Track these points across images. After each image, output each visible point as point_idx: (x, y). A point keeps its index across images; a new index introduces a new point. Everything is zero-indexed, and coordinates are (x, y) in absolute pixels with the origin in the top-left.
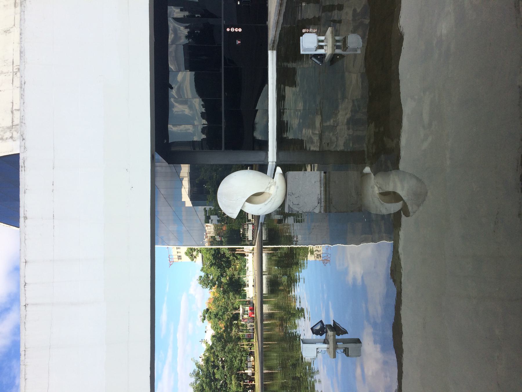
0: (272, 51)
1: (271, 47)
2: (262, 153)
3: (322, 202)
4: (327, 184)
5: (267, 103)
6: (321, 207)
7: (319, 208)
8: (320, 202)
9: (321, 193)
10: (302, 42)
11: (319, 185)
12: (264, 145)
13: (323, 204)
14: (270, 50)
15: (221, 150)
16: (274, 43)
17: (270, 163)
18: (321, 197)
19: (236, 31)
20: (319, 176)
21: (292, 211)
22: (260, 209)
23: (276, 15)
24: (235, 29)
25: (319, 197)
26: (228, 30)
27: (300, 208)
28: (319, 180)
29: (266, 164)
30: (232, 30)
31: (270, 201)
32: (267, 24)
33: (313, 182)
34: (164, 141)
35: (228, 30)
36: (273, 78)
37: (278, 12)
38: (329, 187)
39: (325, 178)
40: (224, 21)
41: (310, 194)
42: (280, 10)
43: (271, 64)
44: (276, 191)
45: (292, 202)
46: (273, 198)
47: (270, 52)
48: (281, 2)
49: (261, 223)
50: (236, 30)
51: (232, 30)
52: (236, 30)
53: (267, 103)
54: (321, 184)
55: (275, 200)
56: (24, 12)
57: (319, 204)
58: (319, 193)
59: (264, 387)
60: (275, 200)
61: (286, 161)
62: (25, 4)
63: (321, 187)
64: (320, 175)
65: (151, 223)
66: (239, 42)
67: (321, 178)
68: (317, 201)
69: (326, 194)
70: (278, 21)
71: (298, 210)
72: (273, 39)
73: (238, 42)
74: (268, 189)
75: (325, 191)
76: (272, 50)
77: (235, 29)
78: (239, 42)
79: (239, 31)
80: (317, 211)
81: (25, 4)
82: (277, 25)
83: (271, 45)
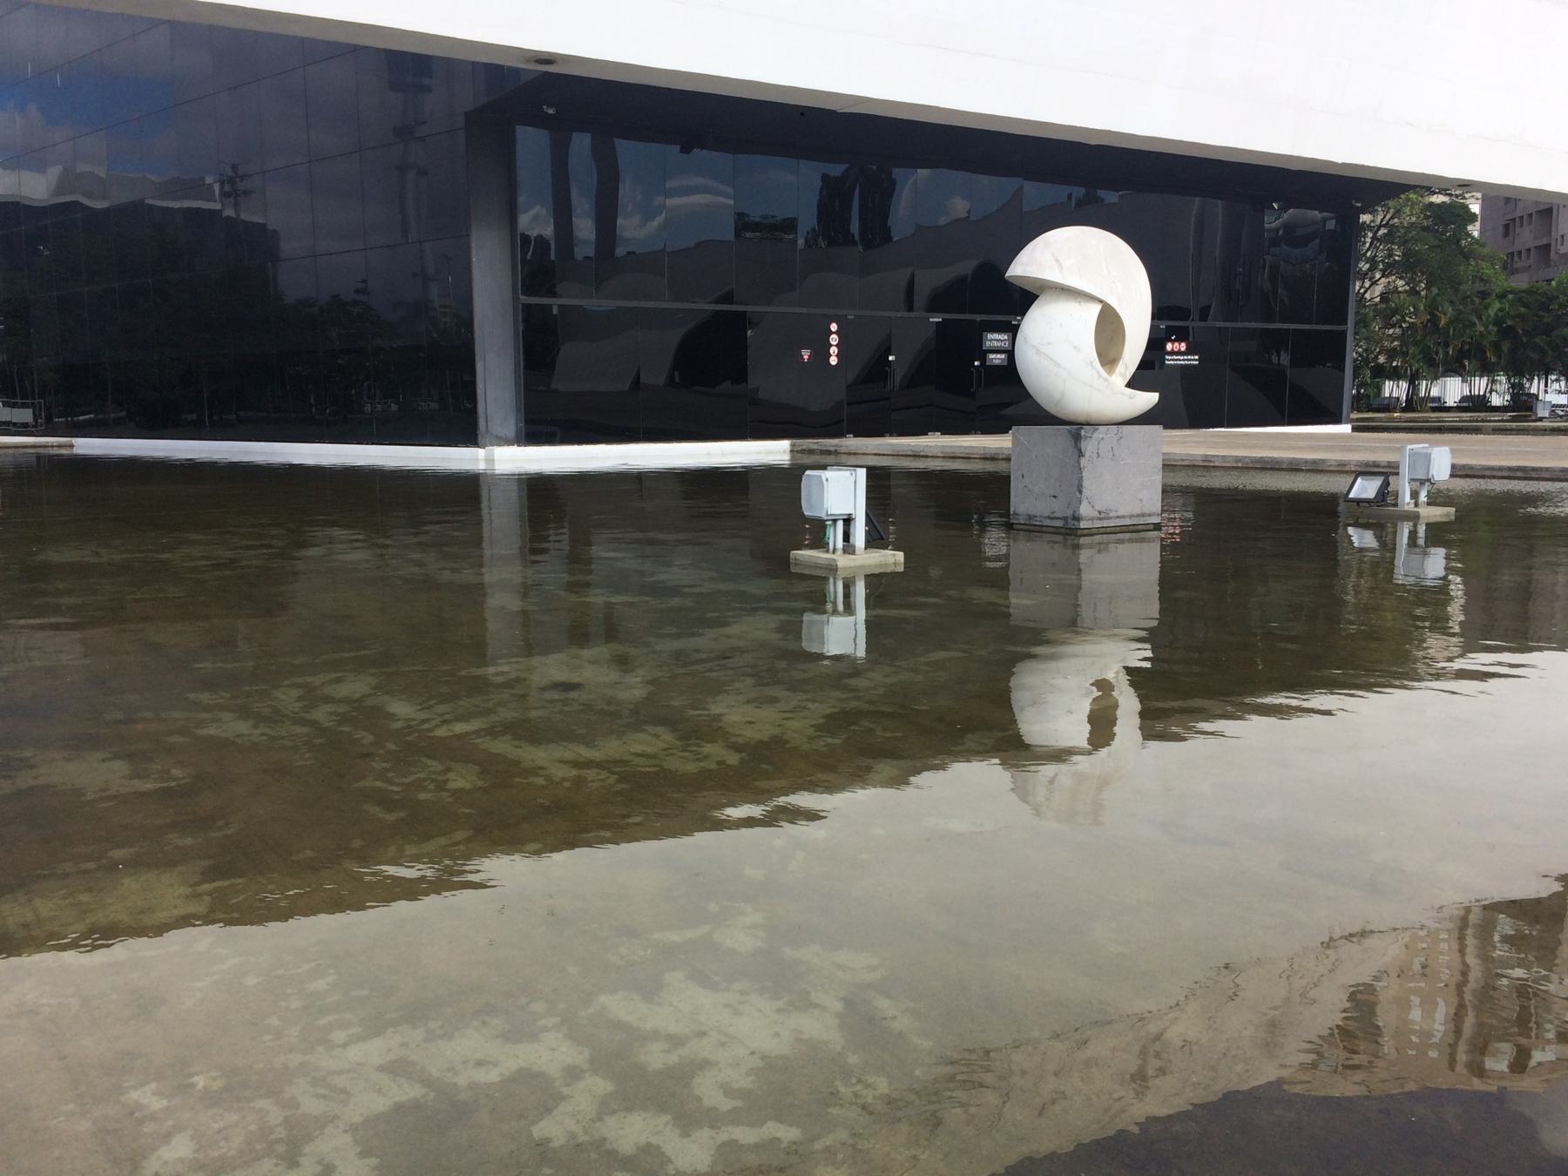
0: (789, 449)
1: (804, 447)
2: (510, 429)
3: (1101, 522)
4: (1135, 531)
5: (376, 442)
6: (1092, 519)
7: (1091, 515)
8: (1103, 515)
9: (1118, 517)
11: (1134, 513)
12: (535, 432)
13: (1098, 524)
15: (527, 291)
18: (1111, 518)
19: (831, 351)
21: (1086, 437)
22: (1075, 348)
23: (948, 450)
24: (832, 345)
25: (1111, 515)
26: (834, 327)
27: (1090, 465)
28: (1146, 511)
29: (480, 439)
30: (834, 339)
31: (1100, 375)
32: (848, 436)
35: (834, 327)
36: (723, 455)
37: (961, 453)
38: (1131, 541)
40: (852, 317)
41: (1118, 488)
42: (969, 458)
45: (1103, 439)
46: (1106, 383)
48: (1002, 459)
49: (72, 446)
50: (834, 350)
51: (834, 339)
52: (834, 350)
53: (376, 442)
54: (1138, 516)
55: (1100, 390)
57: (1098, 515)
58: (1119, 514)
59: (1567, 421)
60: (1100, 390)
61: (489, 496)
63: (1131, 517)
66: (806, 357)
67: (1150, 515)
68: (1104, 510)
70: (923, 456)
72: (844, 448)
73: (806, 354)
76: (792, 451)
77: (832, 345)
78: (806, 357)
82: (906, 456)
83: (816, 447)
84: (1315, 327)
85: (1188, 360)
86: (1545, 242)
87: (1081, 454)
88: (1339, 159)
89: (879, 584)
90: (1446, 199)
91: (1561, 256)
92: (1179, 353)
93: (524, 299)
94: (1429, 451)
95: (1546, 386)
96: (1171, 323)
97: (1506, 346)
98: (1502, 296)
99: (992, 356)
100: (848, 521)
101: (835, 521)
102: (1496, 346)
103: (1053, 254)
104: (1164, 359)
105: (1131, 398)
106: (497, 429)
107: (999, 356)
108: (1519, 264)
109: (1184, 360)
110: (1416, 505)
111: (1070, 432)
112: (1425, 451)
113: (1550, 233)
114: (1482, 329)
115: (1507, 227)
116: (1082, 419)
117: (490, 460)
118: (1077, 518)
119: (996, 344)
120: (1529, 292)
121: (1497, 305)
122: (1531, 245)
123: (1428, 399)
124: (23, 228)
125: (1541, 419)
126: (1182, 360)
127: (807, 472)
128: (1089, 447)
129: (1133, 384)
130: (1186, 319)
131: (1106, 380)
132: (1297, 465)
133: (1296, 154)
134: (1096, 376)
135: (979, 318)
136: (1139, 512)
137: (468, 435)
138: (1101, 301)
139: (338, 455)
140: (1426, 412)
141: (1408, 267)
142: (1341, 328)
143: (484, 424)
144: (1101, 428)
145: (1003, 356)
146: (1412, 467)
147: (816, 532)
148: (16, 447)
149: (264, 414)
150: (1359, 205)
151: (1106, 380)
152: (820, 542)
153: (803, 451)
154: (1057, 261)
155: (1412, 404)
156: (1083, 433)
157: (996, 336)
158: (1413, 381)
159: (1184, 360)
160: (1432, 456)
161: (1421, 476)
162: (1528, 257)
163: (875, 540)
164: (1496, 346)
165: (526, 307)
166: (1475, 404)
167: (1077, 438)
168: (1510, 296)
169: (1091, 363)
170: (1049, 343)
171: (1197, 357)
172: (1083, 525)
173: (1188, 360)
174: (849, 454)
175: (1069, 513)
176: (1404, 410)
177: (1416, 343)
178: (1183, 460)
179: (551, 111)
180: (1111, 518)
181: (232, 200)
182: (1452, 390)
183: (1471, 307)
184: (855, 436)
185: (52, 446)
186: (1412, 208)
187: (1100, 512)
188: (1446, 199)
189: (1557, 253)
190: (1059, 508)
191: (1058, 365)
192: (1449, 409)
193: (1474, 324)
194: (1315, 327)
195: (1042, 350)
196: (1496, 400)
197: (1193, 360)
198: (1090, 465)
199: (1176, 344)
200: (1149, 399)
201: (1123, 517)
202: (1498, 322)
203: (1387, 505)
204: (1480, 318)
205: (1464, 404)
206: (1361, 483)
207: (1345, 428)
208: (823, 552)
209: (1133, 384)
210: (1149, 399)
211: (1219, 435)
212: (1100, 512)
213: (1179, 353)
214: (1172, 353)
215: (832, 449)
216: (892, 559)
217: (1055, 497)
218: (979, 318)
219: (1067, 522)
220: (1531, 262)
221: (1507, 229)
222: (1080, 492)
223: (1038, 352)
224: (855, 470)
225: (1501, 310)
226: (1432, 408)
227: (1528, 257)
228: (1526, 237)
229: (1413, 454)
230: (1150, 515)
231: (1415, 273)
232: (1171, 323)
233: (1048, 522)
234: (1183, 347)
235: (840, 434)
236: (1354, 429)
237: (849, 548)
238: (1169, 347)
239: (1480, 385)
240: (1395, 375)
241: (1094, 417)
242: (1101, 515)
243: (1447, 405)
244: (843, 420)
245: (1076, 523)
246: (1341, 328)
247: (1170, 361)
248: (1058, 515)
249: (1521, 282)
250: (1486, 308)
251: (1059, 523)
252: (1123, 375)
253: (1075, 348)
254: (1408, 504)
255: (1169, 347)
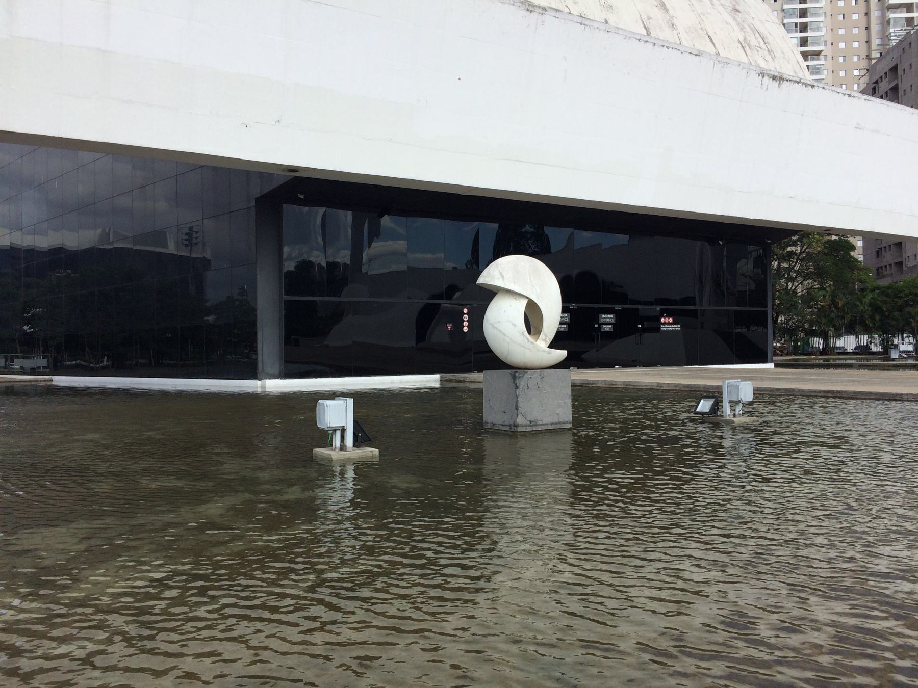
2: (276, 370)
4: (554, 432)
6: (526, 426)
8: (532, 423)
9: (544, 424)
10: (793, 374)
13: (529, 429)
14: (441, 377)
15: (287, 293)
16: (460, 381)
17: (259, 383)
18: (538, 425)
19: (464, 324)
20: (567, 420)
21: (520, 377)
22: (513, 324)
26: (465, 311)
27: (523, 392)
28: (561, 420)
30: (466, 317)
33: (558, 411)
34: (301, 194)
35: (465, 311)
39: (563, 430)
43: (421, 379)
44: (544, 351)
47: (437, 377)
49: (52, 381)
50: (466, 323)
51: (466, 317)
52: (466, 323)
54: (556, 423)
55: (529, 349)
56: (513, 5)
57: (529, 423)
58: (544, 423)
60: (529, 349)
62: (522, 8)
63: (552, 424)
64: (567, 422)
65: (175, 151)
66: (449, 327)
67: (564, 423)
68: (533, 420)
69: (540, 432)
71: (521, 387)
74: (544, 338)
75: (550, 432)
78: (449, 327)
79: (465, 328)
80: (520, 420)
81: (522, 8)
84: (748, 309)
85: (674, 327)
86: (899, 260)
87: (517, 387)
88: (751, 216)
89: (362, 467)
90: (837, 238)
91: (909, 268)
92: (669, 324)
93: (285, 297)
94: (738, 384)
95: (903, 340)
96: (663, 307)
97: (877, 317)
98: (873, 290)
99: (604, 326)
100: (343, 430)
101: (335, 430)
102: (872, 318)
103: (499, 271)
104: (660, 327)
105: (549, 353)
106: (269, 370)
107: (608, 326)
108: (885, 273)
109: (672, 327)
110: (734, 416)
111: (511, 374)
112: (736, 384)
113: (901, 256)
114: (862, 308)
115: (878, 252)
116: (521, 365)
117: (263, 387)
118: (516, 426)
119: (606, 320)
120: (888, 288)
121: (871, 296)
122: (892, 262)
123: (835, 348)
124: (35, 263)
125: (894, 360)
126: (671, 328)
127: (320, 401)
128: (522, 383)
129: (553, 345)
130: (694, 305)
131: (532, 343)
132: (708, 389)
133: (726, 214)
134: (526, 341)
135: (596, 306)
136: (557, 421)
137: (252, 373)
138: (527, 298)
139: (185, 385)
140: (834, 355)
141: (819, 274)
142: (764, 309)
143: (261, 366)
144: (529, 371)
145: (610, 326)
146: (729, 393)
147: (324, 437)
148: (30, 381)
149: (175, 362)
150: (770, 241)
151: (532, 343)
152: (330, 445)
153: (447, 381)
154: (501, 274)
155: (826, 350)
156: (517, 374)
157: (607, 316)
158: (826, 339)
159: (672, 327)
160: (740, 387)
161: (735, 399)
162: (891, 269)
163: (357, 443)
164: (872, 318)
165: (287, 302)
166: (863, 351)
167: (514, 377)
168: (877, 291)
169: (523, 333)
170: (499, 322)
171: (679, 326)
172: (519, 429)
173: (674, 327)
174: (471, 382)
175: (512, 423)
176: (821, 354)
177: (825, 317)
178: (646, 386)
179: (302, 197)
180: (538, 425)
181: (189, 248)
182: (849, 342)
183: (855, 296)
184: (479, 372)
185: (41, 381)
186: (817, 243)
187: (530, 422)
188: (837, 238)
189: (906, 266)
190: (506, 419)
191: (504, 334)
192: (848, 353)
193: (857, 306)
194: (748, 309)
195: (495, 326)
196: (875, 349)
197: (677, 327)
198: (523, 392)
199: (667, 319)
200: (562, 354)
201: (547, 424)
202: (870, 305)
203: (717, 416)
204: (861, 303)
205: (857, 351)
206: (703, 403)
207: (770, 366)
208: (330, 450)
209: (553, 345)
210: (562, 354)
211: (697, 370)
212: (530, 422)
213: (669, 324)
214: (664, 324)
215: (462, 379)
216: (371, 452)
217: (505, 412)
218: (596, 306)
219: (511, 428)
220: (893, 271)
221: (878, 253)
222: (517, 410)
223: (493, 327)
224: (346, 400)
225: (873, 298)
226: (837, 353)
227: (891, 269)
228: (889, 258)
229: (729, 385)
230: (564, 423)
231: (823, 279)
232: (663, 307)
233: (501, 428)
234: (671, 320)
235: (469, 370)
236: (777, 366)
237: (343, 447)
238: (663, 320)
239: (864, 340)
240: (814, 334)
241: (529, 365)
242: (532, 423)
243: (848, 351)
244: (471, 362)
245: (515, 428)
246: (764, 309)
247: (663, 327)
248: (507, 423)
249: (884, 283)
250: (864, 297)
251: (507, 428)
252: (545, 340)
253: (513, 324)
254: (729, 415)
255: (663, 320)
